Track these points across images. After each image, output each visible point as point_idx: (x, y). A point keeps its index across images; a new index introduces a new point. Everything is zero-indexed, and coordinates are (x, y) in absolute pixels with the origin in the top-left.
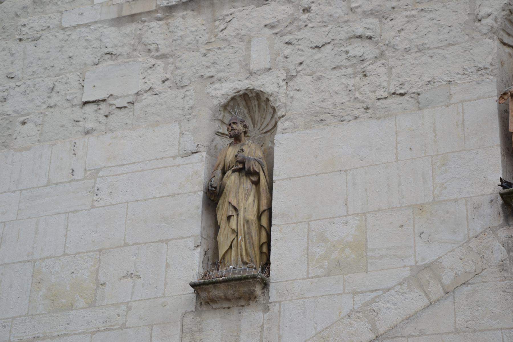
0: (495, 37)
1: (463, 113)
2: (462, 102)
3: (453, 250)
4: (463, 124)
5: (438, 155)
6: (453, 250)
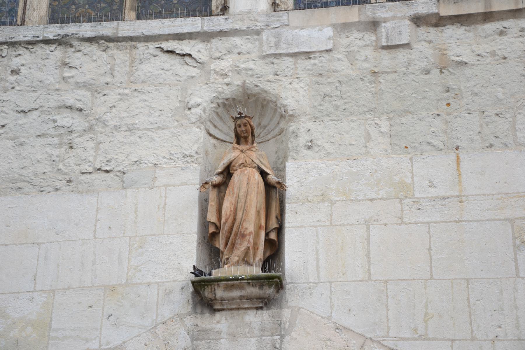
0: (203, 127)
1: (166, 197)
2: (166, 186)
3: (139, 335)
4: (164, 208)
5: (136, 236)
6: (139, 335)
